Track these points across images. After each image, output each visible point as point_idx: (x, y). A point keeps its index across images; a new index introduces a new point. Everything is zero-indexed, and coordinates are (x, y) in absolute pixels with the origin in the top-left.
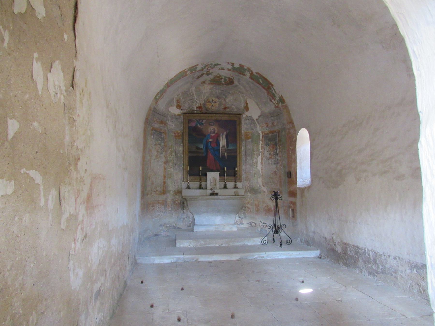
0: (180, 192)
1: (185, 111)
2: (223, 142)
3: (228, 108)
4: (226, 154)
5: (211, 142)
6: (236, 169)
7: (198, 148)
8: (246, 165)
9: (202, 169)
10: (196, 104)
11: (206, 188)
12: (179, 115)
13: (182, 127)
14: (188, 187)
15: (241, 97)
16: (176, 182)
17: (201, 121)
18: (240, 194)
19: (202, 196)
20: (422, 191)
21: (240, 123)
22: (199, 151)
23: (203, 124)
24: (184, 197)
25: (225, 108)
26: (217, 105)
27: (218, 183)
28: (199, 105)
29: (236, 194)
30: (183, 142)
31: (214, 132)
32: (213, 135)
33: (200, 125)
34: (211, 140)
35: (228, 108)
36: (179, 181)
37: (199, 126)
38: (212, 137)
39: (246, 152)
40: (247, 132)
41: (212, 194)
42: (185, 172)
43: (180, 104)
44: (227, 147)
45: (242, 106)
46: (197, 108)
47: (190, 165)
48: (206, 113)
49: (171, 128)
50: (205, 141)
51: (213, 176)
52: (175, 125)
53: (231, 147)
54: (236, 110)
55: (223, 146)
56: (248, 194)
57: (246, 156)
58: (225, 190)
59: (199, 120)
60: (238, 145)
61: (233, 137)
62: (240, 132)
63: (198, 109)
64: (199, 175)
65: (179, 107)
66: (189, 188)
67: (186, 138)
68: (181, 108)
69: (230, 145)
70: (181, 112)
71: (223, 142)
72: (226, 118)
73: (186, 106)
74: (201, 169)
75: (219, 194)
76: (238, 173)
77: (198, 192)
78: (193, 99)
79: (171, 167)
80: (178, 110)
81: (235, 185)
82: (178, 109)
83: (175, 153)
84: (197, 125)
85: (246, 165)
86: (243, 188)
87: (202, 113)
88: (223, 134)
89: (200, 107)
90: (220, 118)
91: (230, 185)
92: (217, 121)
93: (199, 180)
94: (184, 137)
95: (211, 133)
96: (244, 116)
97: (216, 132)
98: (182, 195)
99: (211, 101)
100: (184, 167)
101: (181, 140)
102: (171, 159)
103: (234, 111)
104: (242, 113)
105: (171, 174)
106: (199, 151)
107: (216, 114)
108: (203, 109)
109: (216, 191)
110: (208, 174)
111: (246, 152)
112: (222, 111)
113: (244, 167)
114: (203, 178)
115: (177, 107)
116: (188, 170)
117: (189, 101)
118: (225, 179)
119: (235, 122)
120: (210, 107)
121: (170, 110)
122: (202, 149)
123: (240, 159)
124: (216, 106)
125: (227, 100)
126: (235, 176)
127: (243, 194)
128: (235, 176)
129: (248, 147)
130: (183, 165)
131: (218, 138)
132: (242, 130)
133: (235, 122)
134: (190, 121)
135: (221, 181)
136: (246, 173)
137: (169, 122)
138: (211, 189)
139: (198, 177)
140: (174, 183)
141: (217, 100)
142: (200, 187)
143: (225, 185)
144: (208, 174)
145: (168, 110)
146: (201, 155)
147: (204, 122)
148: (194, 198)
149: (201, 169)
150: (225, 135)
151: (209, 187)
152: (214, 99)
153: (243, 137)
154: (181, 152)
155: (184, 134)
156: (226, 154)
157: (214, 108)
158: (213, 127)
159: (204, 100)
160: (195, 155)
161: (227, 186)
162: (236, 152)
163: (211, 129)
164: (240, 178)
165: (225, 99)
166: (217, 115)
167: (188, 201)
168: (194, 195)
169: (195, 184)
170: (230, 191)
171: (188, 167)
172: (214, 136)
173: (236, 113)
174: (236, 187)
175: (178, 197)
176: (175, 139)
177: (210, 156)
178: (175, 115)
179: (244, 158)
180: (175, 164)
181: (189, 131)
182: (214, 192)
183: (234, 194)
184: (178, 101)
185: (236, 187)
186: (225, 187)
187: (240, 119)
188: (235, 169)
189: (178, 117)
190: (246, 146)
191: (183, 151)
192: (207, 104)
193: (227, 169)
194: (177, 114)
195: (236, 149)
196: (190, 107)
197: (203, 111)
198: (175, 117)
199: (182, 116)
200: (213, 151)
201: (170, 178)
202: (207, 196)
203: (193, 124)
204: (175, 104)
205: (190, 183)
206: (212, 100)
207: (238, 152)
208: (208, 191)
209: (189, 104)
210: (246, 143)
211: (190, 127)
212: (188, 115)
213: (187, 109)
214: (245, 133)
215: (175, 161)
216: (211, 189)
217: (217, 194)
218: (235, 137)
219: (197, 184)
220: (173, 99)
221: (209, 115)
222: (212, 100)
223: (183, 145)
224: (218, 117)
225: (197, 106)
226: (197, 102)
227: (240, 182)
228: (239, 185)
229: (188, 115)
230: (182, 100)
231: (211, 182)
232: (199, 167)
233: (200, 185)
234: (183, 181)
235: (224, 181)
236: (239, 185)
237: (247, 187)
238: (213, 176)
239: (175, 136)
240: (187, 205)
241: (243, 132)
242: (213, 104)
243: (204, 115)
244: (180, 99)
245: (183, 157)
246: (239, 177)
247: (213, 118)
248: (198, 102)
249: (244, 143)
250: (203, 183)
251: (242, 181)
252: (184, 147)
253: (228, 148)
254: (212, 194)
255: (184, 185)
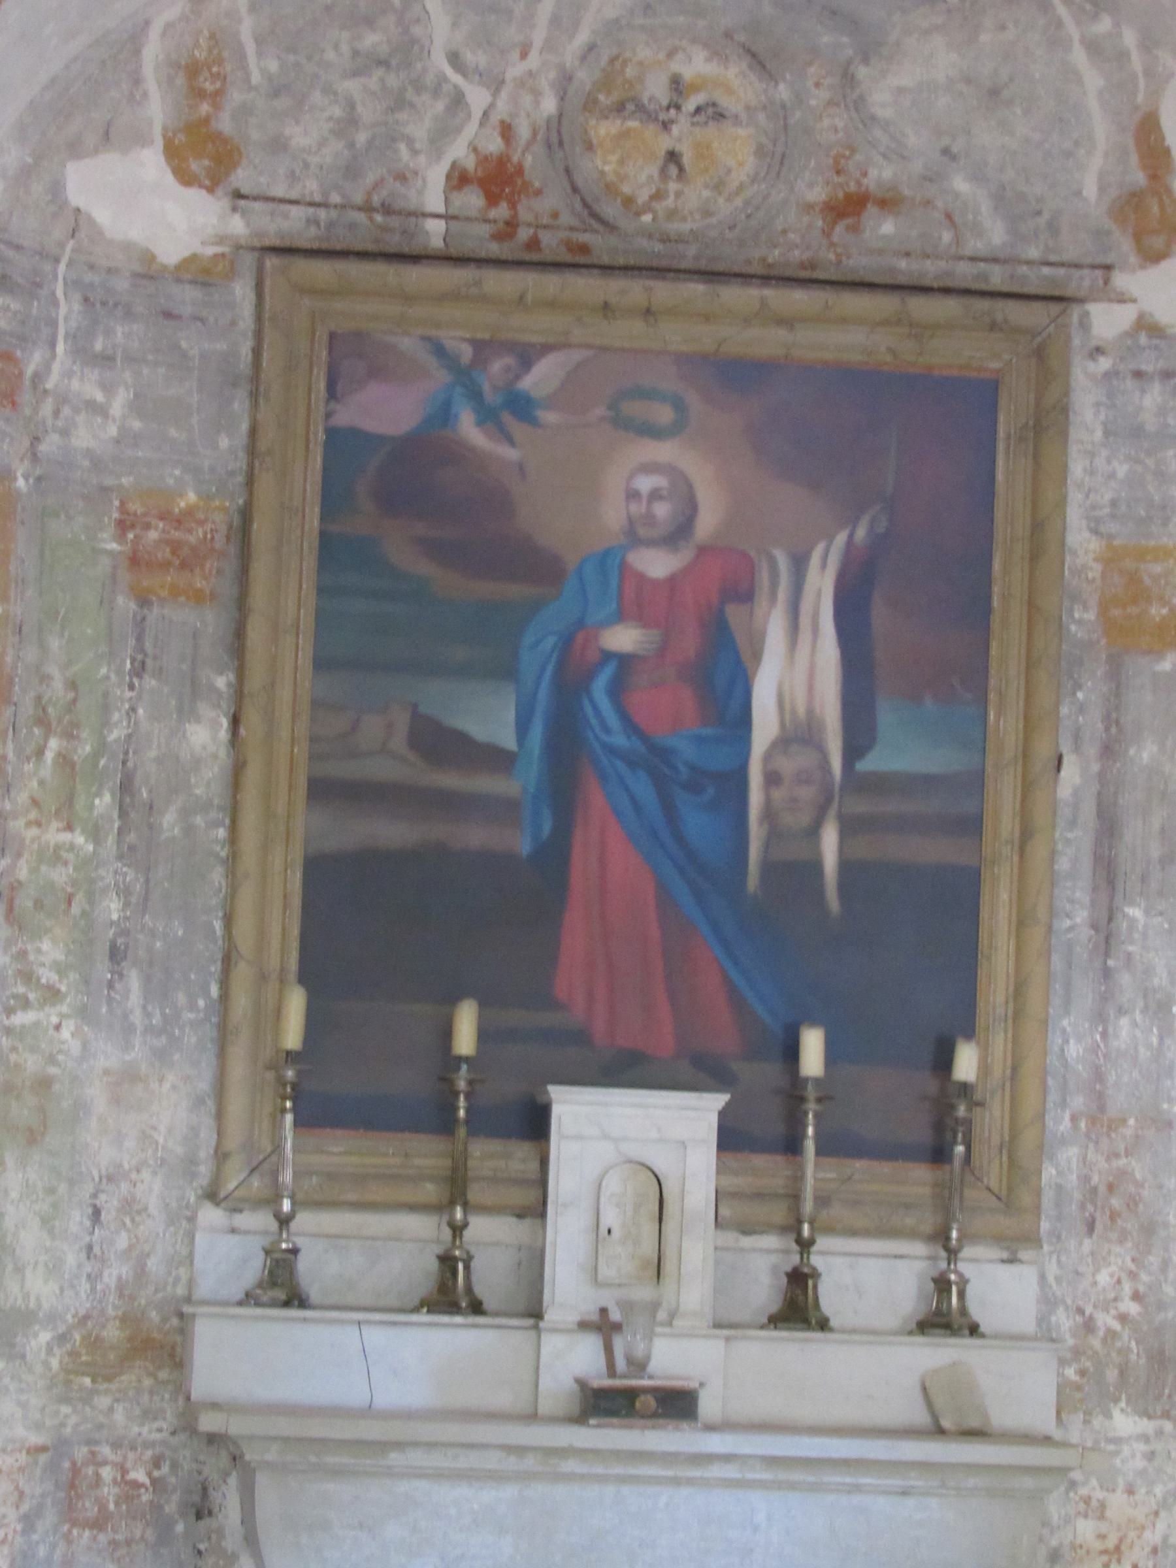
0: (155, 1345)
1: (293, 224)
2: (793, 672)
3: (889, 202)
4: (830, 841)
5: (625, 662)
6: (966, 1063)
7: (438, 743)
8: (1100, 1017)
9: (484, 1035)
10: (442, 134)
11: (535, 1313)
12: (201, 273)
13: (228, 445)
14: (281, 1286)
15: (1079, 56)
16: (110, 1203)
17: (497, 366)
18: (1001, 1417)
19: (467, 1415)
20: (402, 1130)
21: (1048, 423)
22: (450, 780)
23: (521, 407)
24: (208, 1422)
25: (848, 207)
26: (736, 152)
27: (696, 1250)
28: (494, 145)
29: (949, 1419)
30: (237, 646)
31: (679, 532)
32: (657, 564)
33: (487, 416)
34: (623, 638)
35: (889, 202)
36: (152, 1189)
37: (469, 429)
38: (638, 601)
39: (1108, 826)
40: (1141, 554)
41: (606, 1402)
42: (238, 1069)
43: (225, 124)
44: (853, 750)
45: (1090, 190)
46: (459, 179)
47: (324, 968)
48: (577, 260)
49: (83, 439)
50: (538, 648)
51: (630, 1146)
52: (138, 405)
53: (898, 753)
54: (996, 234)
55: (799, 735)
56: (1124, 1422)
57: (1107, 874)
58: (793, 1350)
59: (483, 348)
60: (1005, 725)
61: (940, 598)
62: (1042, 536)
63: (472, 200)
64: (444, 1124)
65: (203, 154)
66: (295, 1299)
67: (288, 589)
68: (242, 178)
69: (887, 716)
70: (237, 226)
71: (793, 672)
72: (849, 334)
73: (304, 155)
74: (465, 1041)
75: (709, 1406)
76: (991, 1122)
77: (418, 1363)
78: (408, 50)
79: (53, 995)
80: (195, 195)
81: (942, 1285)
82: (186, 178)
83: (126, 787)
84: (444, 415)
85: (1100, 1017)
86: (1046, 1335)
87: (532, 261)
88: (799, 564)
89: (496, 179)
90: (768, 342)
91: (870, 1277)
92: (734, 375)
93: (430, 1191)
94: (261, 569)
95: (633, 538)
96: (1107, 321)
97: (707, 523)
98: (181, 1389)
99: (656, 89)
100: (241, 1003)
101: (211, 622)
102: (60, 876)
103: (974, 245)
104: (1084, 280)
105: (44, 1084)
106: (450, 780)
107: (712, 276)
108: (546, 207)
109: (671, 1358)
110: (574, 1110)
111: (1108, 826)
112: (797, 235)
113: (1071, 1042)
114: (488, 1156)
115: (173, 154)
116: (293, 1037)
117: (352, 86)
118: (795, 1198)
119: (983, 394)
120: (641, 178)
121: (76, 196)
122: (497, 759)
123: (1021, 923)
124: (726, 179)
125: (882, 93)
126: (939, 1155)
127: (1043, 1419)
128: (939, 1155)
129: (1145, 753)
130: (228, 961)
131: (734, 614)
132: (1074, 515)
133: (983, 394)
134: (350, 358)
135: (734, 1213)
136: (1100, 1120)
137: (57, 367)
138: (604, 1326)
139: (426, 1153)
140: (77, 1219)
141: (737, 85)
142: (450, 1293)
143: (800, 1281)
144: (574, 1110)
145: (57, 190)
146: (475, 836)
147: (541, 378)
148: (354, 1445)
149: (465, 1041)
150: (821, 584)
151: (568, 1290)
152: (696, 65)
153: (1082, 620)
154: (209, 781)
155: (262, 529)
156: (830, 841)
157: (695, 194)
158: (664, 451)
159: (564, 81)
160: (392, 832)
161: (831, 1296)
162: (971, 826)
163: (638, 489)
164: (1007, 1202)
165: (848, 78)
166: (736, 296)
167: (262, 1480)
168: (354, 1393)
169: (370, 1244)
170: (867, 1369)
171: (296, 1004)
172: (672, 582)
173: (997, 278)
174: (944, 1317)
175: (126, 1417)
176: (125, 604)
177: (612, 856)
178: (149, 271)
179: (1076, 916)
180: (116, 955)
181: (335, 498)
182: (639, 1366)
183: (919, 1417)
184: (201, 75)
185: (944, 1317)
186: (798, 1307)
187: (1046, 362)
188: (944, 1061)
189: (187, 297)
190: (1109, 751)
191: (238, 769)
192: (604, 129)
193: (832, 1055)
194: (170, 253)
195: (975, 783)
196: (352, 171)
197: (536, 229)
198: (153, 291)
199: (242, 291)
200: (643, 788)
201: (33, 1138)
202: (532, 1417)
203: (387, 410)
204: (157, 109)
205: (305, 1221)
206: (676, 83)
207: (1003, 820)
208: (551, 1344)
209: (350, 121)
210: (1112, 719)
211: (343, 446)
212: (322, 271)
213: (311, 187)
214: (1111, 559)
215: (113, 908)
216: (604, 1326)
217: (677, 1404)
218: (976, 611)
219: (406, 1242)
220: (135, 40)
221: (635, 290)
222: (676, 83)
223: (239, 693)
224: (740, 322)
225: (459, 151)
226: (458, 100)
227: (1016, 1244)
228: (998, 1287)
229: (330, 272)
230: (261, 67)
231: (599, 1233)
232: (452, 1000)
233: (447, 1261)
234: (212, 1195)
235: (941, 1237)
236: (998, 1287)
237: (1106, 1320)
238: (630, 1146)
239: (134, 560)
240: (251, 1539)
241: (1081, 543)
242: (683, 135)
243: (551, 283)
244: (220, 40)
245: (232, 861)
246: (993, 1172)
247: (676, 336)
248: (477, 98)
249: (1082, 705)
250: (490, 1236)
251: (1032, 1239)
252: (253, 719)
253: (867, 765)
254: (606, 1402)
255: (226, 1251)
